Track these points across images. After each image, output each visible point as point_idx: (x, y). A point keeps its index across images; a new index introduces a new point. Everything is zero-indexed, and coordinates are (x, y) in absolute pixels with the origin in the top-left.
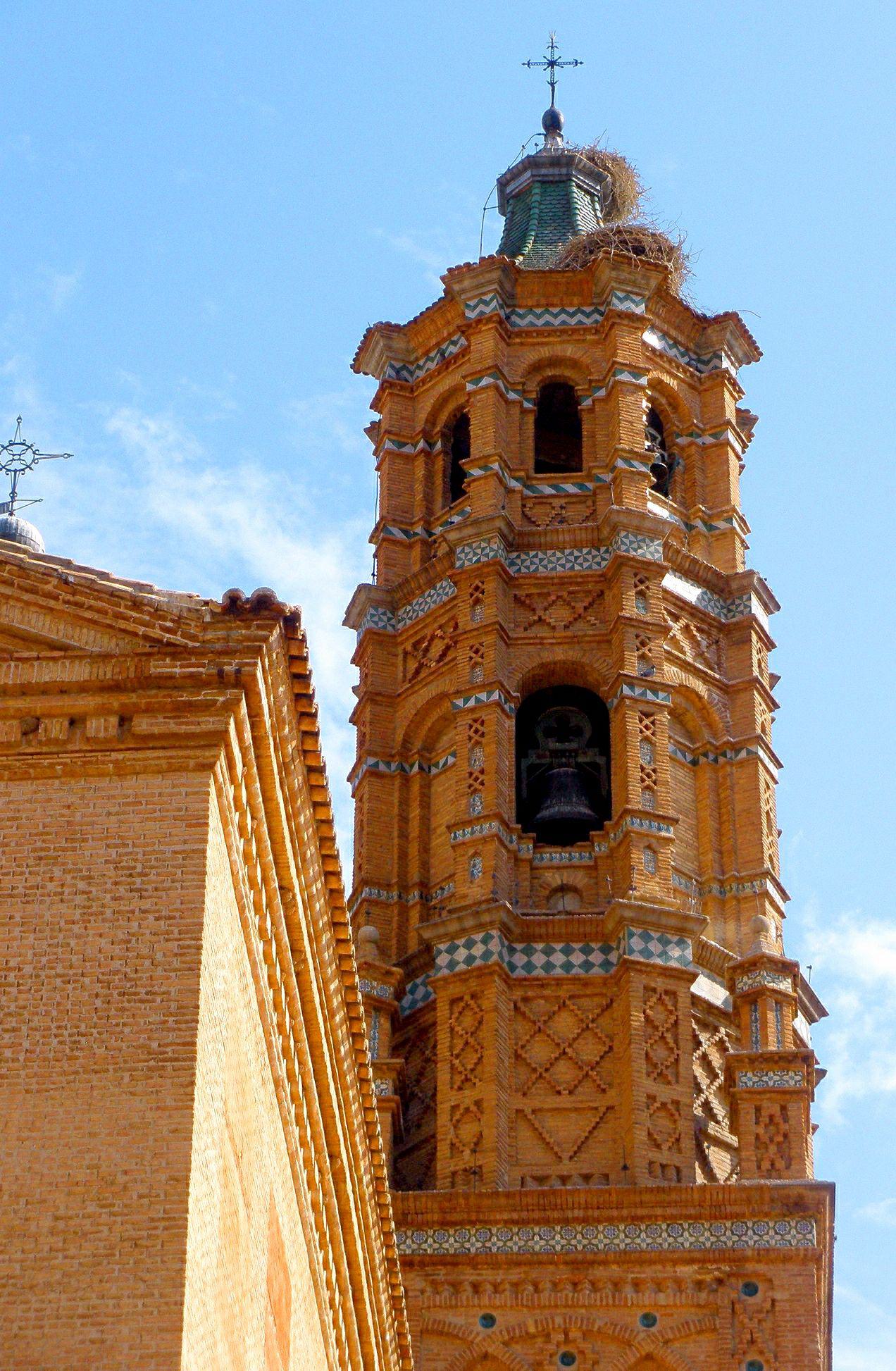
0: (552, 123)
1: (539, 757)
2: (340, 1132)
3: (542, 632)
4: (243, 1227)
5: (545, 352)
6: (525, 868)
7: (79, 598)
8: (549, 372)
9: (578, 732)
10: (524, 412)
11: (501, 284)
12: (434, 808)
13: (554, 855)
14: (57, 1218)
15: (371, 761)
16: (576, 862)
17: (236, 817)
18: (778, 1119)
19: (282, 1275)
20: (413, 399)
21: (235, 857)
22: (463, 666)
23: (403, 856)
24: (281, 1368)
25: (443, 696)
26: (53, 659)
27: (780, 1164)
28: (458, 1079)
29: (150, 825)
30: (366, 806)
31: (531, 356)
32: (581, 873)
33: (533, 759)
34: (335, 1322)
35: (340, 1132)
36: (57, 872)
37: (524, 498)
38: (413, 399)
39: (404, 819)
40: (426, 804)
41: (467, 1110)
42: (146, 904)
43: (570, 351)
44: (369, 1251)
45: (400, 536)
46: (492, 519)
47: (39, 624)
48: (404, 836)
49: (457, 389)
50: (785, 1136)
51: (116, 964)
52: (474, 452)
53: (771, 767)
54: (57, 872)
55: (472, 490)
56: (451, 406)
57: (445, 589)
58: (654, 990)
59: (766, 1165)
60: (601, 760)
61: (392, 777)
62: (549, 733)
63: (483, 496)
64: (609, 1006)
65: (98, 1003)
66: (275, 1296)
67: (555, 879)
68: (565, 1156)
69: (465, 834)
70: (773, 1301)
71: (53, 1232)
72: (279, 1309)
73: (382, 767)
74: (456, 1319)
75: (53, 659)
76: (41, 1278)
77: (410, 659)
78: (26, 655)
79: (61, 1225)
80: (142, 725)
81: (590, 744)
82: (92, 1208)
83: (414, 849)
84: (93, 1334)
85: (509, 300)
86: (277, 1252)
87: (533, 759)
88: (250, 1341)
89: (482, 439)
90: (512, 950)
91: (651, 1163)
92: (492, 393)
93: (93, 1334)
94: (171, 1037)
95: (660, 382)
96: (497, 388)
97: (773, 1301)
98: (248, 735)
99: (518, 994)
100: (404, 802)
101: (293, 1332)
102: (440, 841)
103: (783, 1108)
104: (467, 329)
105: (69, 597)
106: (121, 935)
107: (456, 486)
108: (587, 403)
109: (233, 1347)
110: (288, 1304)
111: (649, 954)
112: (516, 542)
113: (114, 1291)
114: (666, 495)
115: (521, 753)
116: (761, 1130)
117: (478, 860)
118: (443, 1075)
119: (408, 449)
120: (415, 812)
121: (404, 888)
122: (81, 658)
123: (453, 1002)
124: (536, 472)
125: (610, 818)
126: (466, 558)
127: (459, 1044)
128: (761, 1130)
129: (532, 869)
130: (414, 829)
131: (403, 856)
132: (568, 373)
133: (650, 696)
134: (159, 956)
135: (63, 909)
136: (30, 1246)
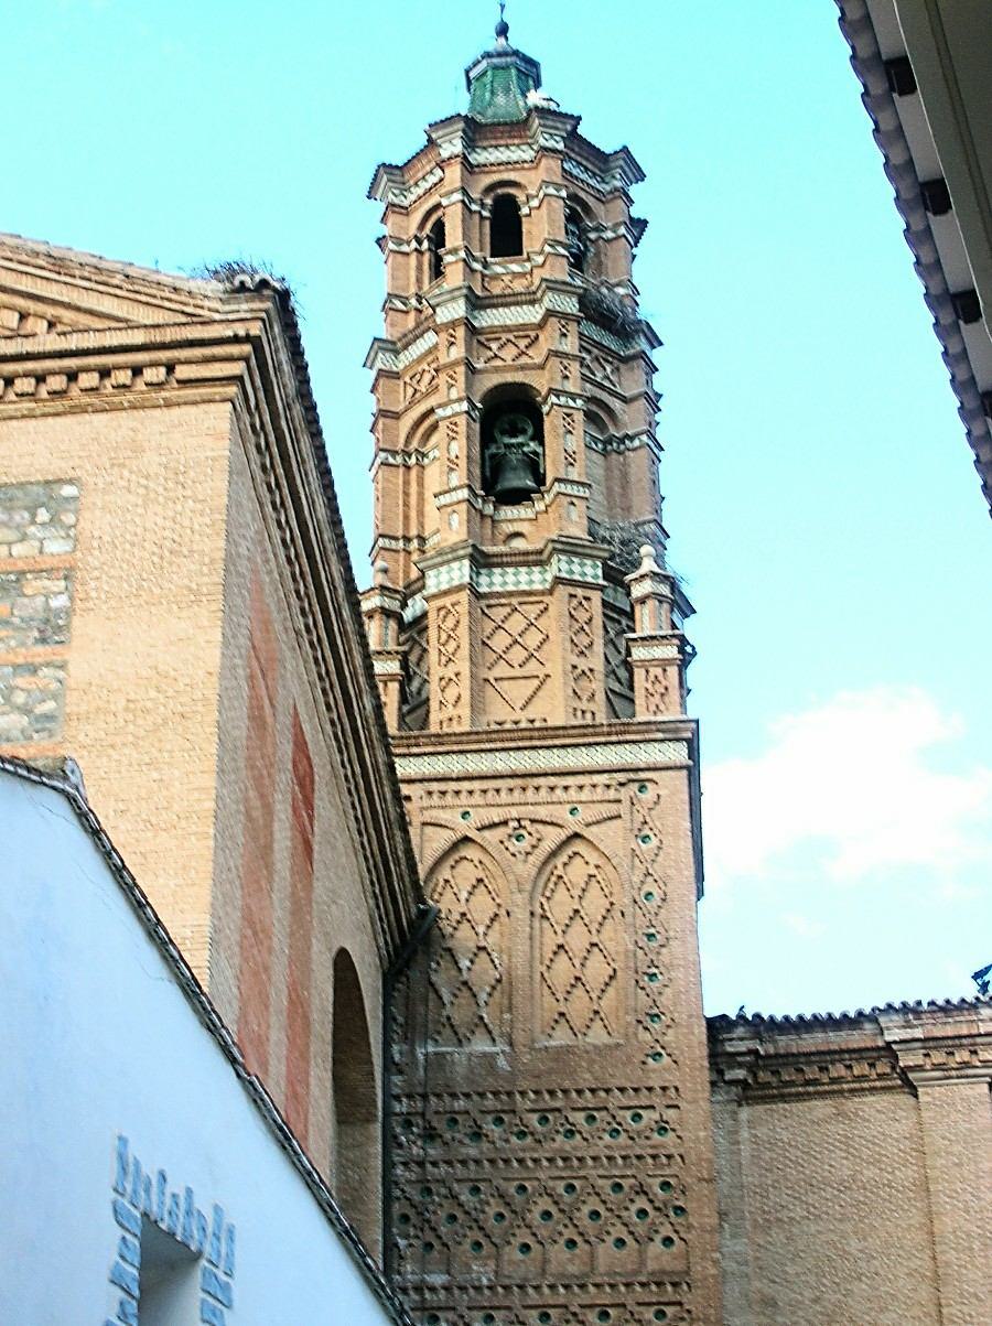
0: (503, 30)
1: (498, 448)
2: (347, 673)
3: (498, 363)
4: (269, 720)
5: (496, 177)
6: (489, 521)
7: (136, 288)
8: (500, 191)
9: (524, 432)
10: (482, 218)
11: (464, 131)
12: (426, 486)
13: (508, 512)
14: (128, 701)
15: (382, 455)
16: (523, 516)
17: (253, 439)
18: (661, 678)
19: (305, 761)
20: (407, 214)
21: (253, 466)
22: (443, 387)
23: (406, 517)
24: (4, 254)
25: (431, 411)
26: (120, 329)
27: (662, 707)
28: (444, 659)
29: (189, 440)
30: (380, 486)
31: (487, 180)
32: (526, 524)
33: (493, 450)
34: (353, 804)
35: (347, 673)
36: (126, 473)
37: (483, 276)
38: (407, 214)
39: (406, 494)
40: (421, 484)
41: (450, 680)
42: (189, 493)
43: (512, 176)
44: (373, 756)
45: (400, 306)
46: (460, 288)
47: (107, 305)
48: (406, 505)
49: (438, 206)
50: (666, 689)
51: (167, 533)
52: (448, 245)
53: (656, 450)
54: (126, 473)
55: (448, 271)
56: (434, 218)
57: (430, 338)
58: (575, 596)
59: (653, 708)
60: (540, 450)
61: (398, 466)
62: (504, 433)
63: (454, 276)
64: (546, 609)
65: (156, 559)
66: (302, 772)
67: (509, 528)
68: (517, 708)
69: (444, 500)
70: (659, 796)
71: (127, 709)
72: (305, 782)
73: (391, 460)
74: (442, 816)
75: (120, 329)
76: (118, 740)
77: (408, 387)
78: (100, 326)
79: (132, 706)
80: (182, 372)
81: (532, 439)
82: (153, 694)
83: (413, 514)
84: (155, 775)
85: (471, 143)
86: (300, 745)
87: (493, 450)
88: (279, 796)
89: (454, 237)
90: (478, 574)
91: (575, 709)
92: (460, 205)
93: (155, 775)
94: (206, 579)
95: (576, 196)
96: (463, 202)
97: (659, 796)
98: (258, 382)
99: (483, 603)
100: (406, 483)
101: (317, 802)
102: (431, 505)
103: (665, 670)
104: (441, 165)
105: (131, 287)
106: (171, 514)
107: (438, 271)
108: (525, 210)
109: (262, 796)
110: (312, 782)
111: (572, 572)
112: (476, 303)
113: (169, 747)
114: (582, 272)
115: (484, 445)
116: (649, 686)
117: (455, 516)
118: (433, 656)
119: (405, 248)
120: (414, 489)
121: (407, 539)
122: (138, 327)
123: (439, 610)
124: (492, 256)
125: (544, 484)
126: (444, 315)
127: (444, 637)
128: (649, 686)
129: (493, 521)
130: (413, 500)
131: (406, 517)
132: (512, 191)
133: (571, 403)
134: (196, 527)
135: (132, 498)
136: (111, 718)
